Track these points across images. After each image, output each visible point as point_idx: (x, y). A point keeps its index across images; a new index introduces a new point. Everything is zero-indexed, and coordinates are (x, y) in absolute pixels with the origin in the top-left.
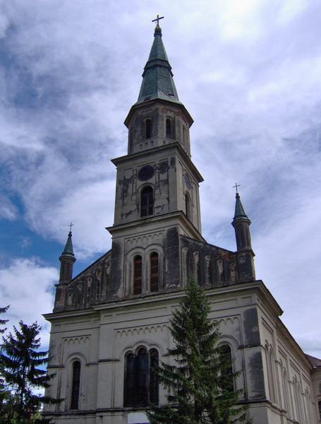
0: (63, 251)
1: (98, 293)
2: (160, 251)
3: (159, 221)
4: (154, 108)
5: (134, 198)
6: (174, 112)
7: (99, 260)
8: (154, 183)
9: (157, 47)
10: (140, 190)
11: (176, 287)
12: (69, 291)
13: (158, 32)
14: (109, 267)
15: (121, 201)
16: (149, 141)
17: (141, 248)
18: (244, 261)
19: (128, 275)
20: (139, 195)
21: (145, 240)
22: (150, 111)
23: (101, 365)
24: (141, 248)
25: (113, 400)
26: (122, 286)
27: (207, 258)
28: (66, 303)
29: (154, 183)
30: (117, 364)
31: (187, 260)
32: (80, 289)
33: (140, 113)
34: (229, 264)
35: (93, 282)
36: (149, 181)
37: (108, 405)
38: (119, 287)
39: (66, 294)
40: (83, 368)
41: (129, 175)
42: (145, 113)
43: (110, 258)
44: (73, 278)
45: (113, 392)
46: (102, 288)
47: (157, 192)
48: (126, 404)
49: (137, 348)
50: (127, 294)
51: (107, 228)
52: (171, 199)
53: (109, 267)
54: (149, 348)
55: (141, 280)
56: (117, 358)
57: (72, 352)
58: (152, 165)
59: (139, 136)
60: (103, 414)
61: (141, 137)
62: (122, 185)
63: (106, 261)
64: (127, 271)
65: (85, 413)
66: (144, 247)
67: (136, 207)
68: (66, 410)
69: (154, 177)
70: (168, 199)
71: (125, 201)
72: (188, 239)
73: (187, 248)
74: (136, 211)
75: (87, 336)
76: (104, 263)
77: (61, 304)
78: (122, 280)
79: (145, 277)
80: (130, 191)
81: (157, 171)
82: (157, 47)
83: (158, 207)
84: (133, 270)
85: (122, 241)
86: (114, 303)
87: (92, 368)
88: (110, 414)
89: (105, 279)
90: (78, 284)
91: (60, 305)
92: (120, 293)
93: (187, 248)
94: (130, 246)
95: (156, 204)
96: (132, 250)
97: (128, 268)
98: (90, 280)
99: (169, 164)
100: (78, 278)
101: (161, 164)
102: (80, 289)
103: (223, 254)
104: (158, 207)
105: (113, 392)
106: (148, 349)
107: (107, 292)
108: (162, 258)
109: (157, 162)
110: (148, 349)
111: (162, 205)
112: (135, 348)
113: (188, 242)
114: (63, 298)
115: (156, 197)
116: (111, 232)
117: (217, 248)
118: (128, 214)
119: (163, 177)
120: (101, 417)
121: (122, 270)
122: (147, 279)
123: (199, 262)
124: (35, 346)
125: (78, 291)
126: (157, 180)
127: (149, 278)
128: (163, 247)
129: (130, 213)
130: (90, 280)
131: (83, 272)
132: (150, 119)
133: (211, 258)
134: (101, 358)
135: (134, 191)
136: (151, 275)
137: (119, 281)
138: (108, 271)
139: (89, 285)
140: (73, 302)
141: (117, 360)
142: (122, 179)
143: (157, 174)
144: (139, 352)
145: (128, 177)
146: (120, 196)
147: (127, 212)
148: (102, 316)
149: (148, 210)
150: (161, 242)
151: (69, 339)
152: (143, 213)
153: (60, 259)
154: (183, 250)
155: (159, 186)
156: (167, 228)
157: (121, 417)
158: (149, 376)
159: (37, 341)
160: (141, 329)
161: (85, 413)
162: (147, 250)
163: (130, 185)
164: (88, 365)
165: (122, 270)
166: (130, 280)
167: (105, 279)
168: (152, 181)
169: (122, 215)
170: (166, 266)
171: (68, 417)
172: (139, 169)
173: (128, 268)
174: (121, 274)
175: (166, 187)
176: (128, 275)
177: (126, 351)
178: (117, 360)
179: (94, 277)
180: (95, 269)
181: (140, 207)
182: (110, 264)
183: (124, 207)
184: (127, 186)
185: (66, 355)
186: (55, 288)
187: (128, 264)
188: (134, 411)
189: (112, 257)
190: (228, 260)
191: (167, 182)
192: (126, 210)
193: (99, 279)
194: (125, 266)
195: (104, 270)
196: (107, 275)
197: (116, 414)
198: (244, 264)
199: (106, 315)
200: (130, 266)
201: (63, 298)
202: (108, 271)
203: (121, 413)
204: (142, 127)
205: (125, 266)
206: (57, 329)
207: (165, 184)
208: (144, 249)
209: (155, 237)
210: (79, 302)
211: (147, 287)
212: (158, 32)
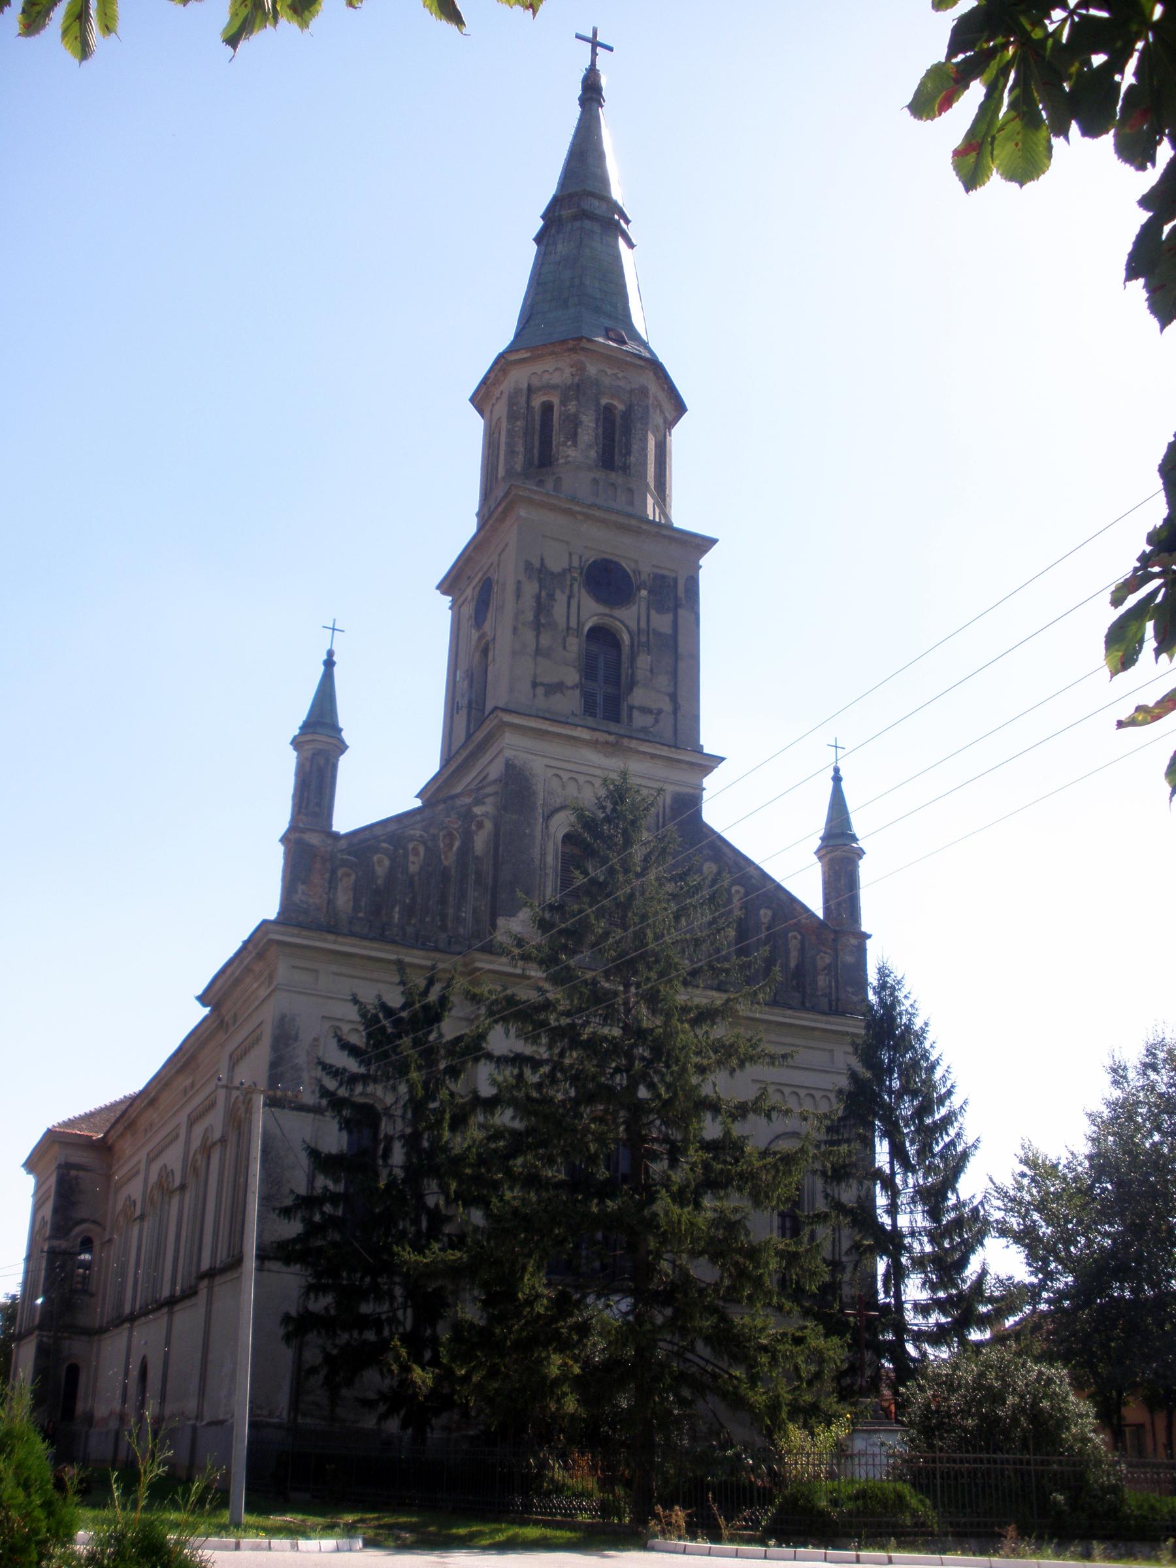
12: (344, 863)
13: (329, 663)
36: (617, 613)
81: (644, 593)
135: (573, 624)
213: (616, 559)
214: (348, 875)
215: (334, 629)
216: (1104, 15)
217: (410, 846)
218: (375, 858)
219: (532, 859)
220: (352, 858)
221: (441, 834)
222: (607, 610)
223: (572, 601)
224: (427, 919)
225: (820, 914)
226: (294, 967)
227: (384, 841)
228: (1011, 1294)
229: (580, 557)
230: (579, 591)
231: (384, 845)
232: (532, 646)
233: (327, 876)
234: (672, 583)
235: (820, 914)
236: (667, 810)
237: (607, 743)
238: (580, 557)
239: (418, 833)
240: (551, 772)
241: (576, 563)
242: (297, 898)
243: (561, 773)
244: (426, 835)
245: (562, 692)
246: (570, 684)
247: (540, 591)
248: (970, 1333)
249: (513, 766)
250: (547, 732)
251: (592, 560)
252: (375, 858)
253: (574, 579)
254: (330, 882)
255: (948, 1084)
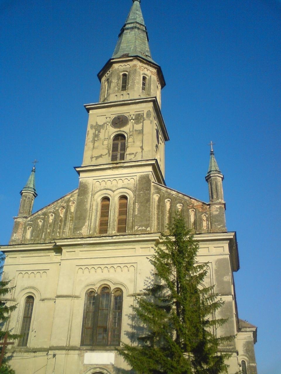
12: (29, 225)
36: (122, 129)
214: (31, 227)
216: (211, 142)
219: (87, 209)
220: (31, 223)
222: (119, 130)
224: (53, 235)
227: (41, 215)
228: (43, 213)
232: (92, 147)
233: (23, 229)
234: (142, 115)
239: (52, 210)
245: (102, 157)
247: (96, 132)
248: (171, 276)
253: (108, 125)
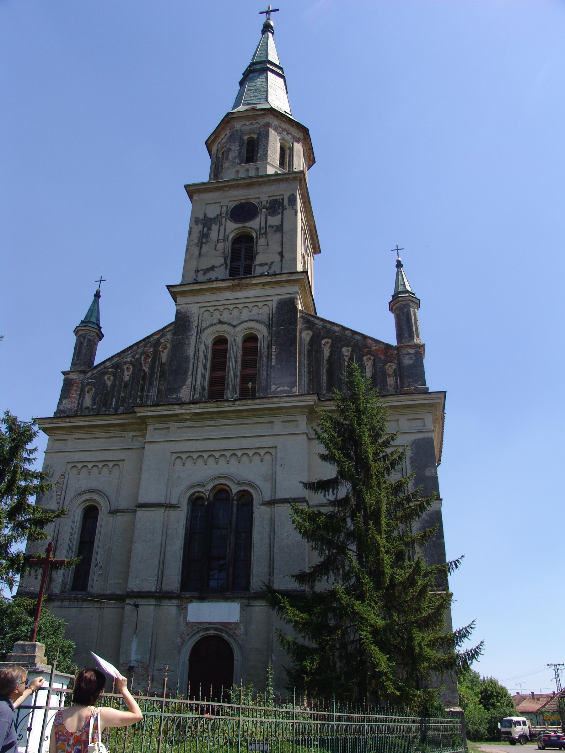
0: (83, 319)
1: (142, 390)
2: (262, 332)
3: (264, 284)
4: (262, 121)
5: (220, 246)
6: (294, 137)
7: (148, 338)
8: (257, 227)
9: (94, 310)
10: (231, 237)
11: (290, 391)
12: (88, 384)
13: (97, 295)
14: (166, 351)
15: (196, 251)
16: (251, 166)
17: (229, 324)
18: (411, 362)
19: (201, 365)
20: (229, 244)
21: (236, 312)
22: (255, 126)
23: (141, 513)
24: (229, 324)
25: (161, 575)
26: (189, 382)
27: (346, 351)
28: (80, 404)
29: (257, 227)
30: (173, 514)
31: (310, 352)
32: (109, 383)
33: (238, 125)
34: (386, 364)
35: (133, 373)
36: (248, 224)
37: (150, 586)
38: (184, 383)
39: (82, 390)
40: (103, 518)
41: (212, 212)
42: (247, 128)
43: (169, 336)
44: (95, 365)
45: (162, 563)
46: (151, 384)
47: (262, 242)
48: (185, 585)
49: (214, 487)
50: (197, 396)
51: (168, 287)
52: (286, 255)
53: (166, 351)
54: (235, 489)
55: (224, 377)
56: (174, 501)
57: (84, 488)
58: (255, 202)
59: (235, 158)
60: (139, 601)
61: (237, 160)
62: (200, 226)
63: (162, 340)
64: (201, 359)
65: (101, 598)
66: (235, 323)
67: (222, 261)
68: (62, 592)
69: (258, 220)
70: (281, 254)
71: (204, 250)
72: (312, 319)
73: (311, 333)
74: (223, 267)
75: (117, 463)
76: (157, 343)
77: (68, 405)
78: (190, 373)
79: (231, 373)
80: (213, 235)
81: (264, 210)
82: (94, 310)
83: (261, 265)
84: (209, 357)
85: (194, 309)
86: (176, 407)
87: (121, 518)
88: (152, 602)
89: (158, 369)
90: (106, 373)
91: (69, 406)
92: (185, 393)
93: (311, 333)
94: (208, 319)
95: (259, 259)
96: (211, 325)
97: (201, 354)
98: (128, 368)
99: (286, 203)
100: (108, 364)
101: (271, 201)
102: (109, 383)
103: (374, 348)
104: (261, 265)
105: (162, 563)
106: (234, 492)
107: (159, 391)
108: (265, 344)
109: (265, 198)
110: (234, 492)
111: (269, 262)
112: (210, 487)
113: (314, 324)
114: (75, 394)
115: (260, 249)
116: (174, 296)
117: (365, 337)
118: (206, 271)
119: (274, 221)
120: (136, 606)
121: (192, 356)
122: (235, 374)
123: (329, 356)
124: (27, 459)
125: (105, 385)
126: (263, 225)
127: (239, 373)
128: (269, 327)
129: (212, 268)
130: (128, 369)
131: (118, 355)
132: (255, 136)
133: (352, 352)
134: (142, 499)
135: (221, 237)
136: (241, 371)
137: (185, 373)
138: (164, 358)
139: (127, 378)
140: (94, 403)
141: (173, 507)
142: (201, 217)
143: (263, 217)
144: (216, 495)
145: (211, 214)
146: (196, 241)
147: (208, 266)
148: (150, 428)
149: (242, 269)
150: (265, 318)
151: (80, 466)
152: (234, 273)
153: (76, 332)
154: (304, 335)
155: (265, 233)
156: (276, 298)
157: (152, 608)
158: (233, 539)
159: (31, 452)
160: (222, 455)
161: (101, 598)
162: (238, 329)
163: (215, 228)
164: (113, 512)
165: (192, 356)
166: (204, 375)
167: (158, 369)
168: (255, 224)
169: (197, 271)
170: (273, 357)
171: (66, 603)
172: (233, 205)
173: (201, 354)
174: (189, 362)
175: (278, 236)
176: (201, 365)
177: (192, 491)
178: (173, 507)
179: (136, 365)
180: (140, 351)
181: (228, 262)
182: (169, 345)
183: (201, 258)
184: (209, 229)
185: (70, 494)
186: (63, 377)
187: (202, 348)
188: (202, 599)
189: (174, 334)
190: (382, 357)
191: (280, 228)
192: (205, 263)
193: (147, 370)
194: (196, 351)
195: (156, 354)
196: (162, 364)
197: (166, 602)
198: (411, 366)
199: (157, 426)
200: (206, 351)
201: (75, 394)
202: (164, 358)
203: (175, 602)
204: (241, 146)
205: (196, 351)
206: (59, 446)
207: (276, 231)
208: (235, 327)
209: (255, 311)
210: (105, 405)
211: (235, 388)
212: (97, 295)
213: (249, 201)
214: (92, 389)
215: (397, 250)
217: (125, 367)
218: (106, 378)
221: (143, 357)
223: (221, 227)
224: (130, 401)
225: (97, 362)
226: (56, 440)
227: (110, 368)
229: (227, 207)
230: (226, 222)
231: (110, 370)
233: (79, 392)
235: (97, 362)
236: (274, 309)
237: (233, 285)
238: (227, 207)
239: (129, 360)
240: (203, 310)
241: (224, 209)
242: (62, 407)
243: (238, 306)
244: (133, 360)
246: (217, 264)
249: (181, 312)
250: (199, 290)
251: (234, 206)
252: (106, 378)
254: (80, 394)
255: (31, 457)
